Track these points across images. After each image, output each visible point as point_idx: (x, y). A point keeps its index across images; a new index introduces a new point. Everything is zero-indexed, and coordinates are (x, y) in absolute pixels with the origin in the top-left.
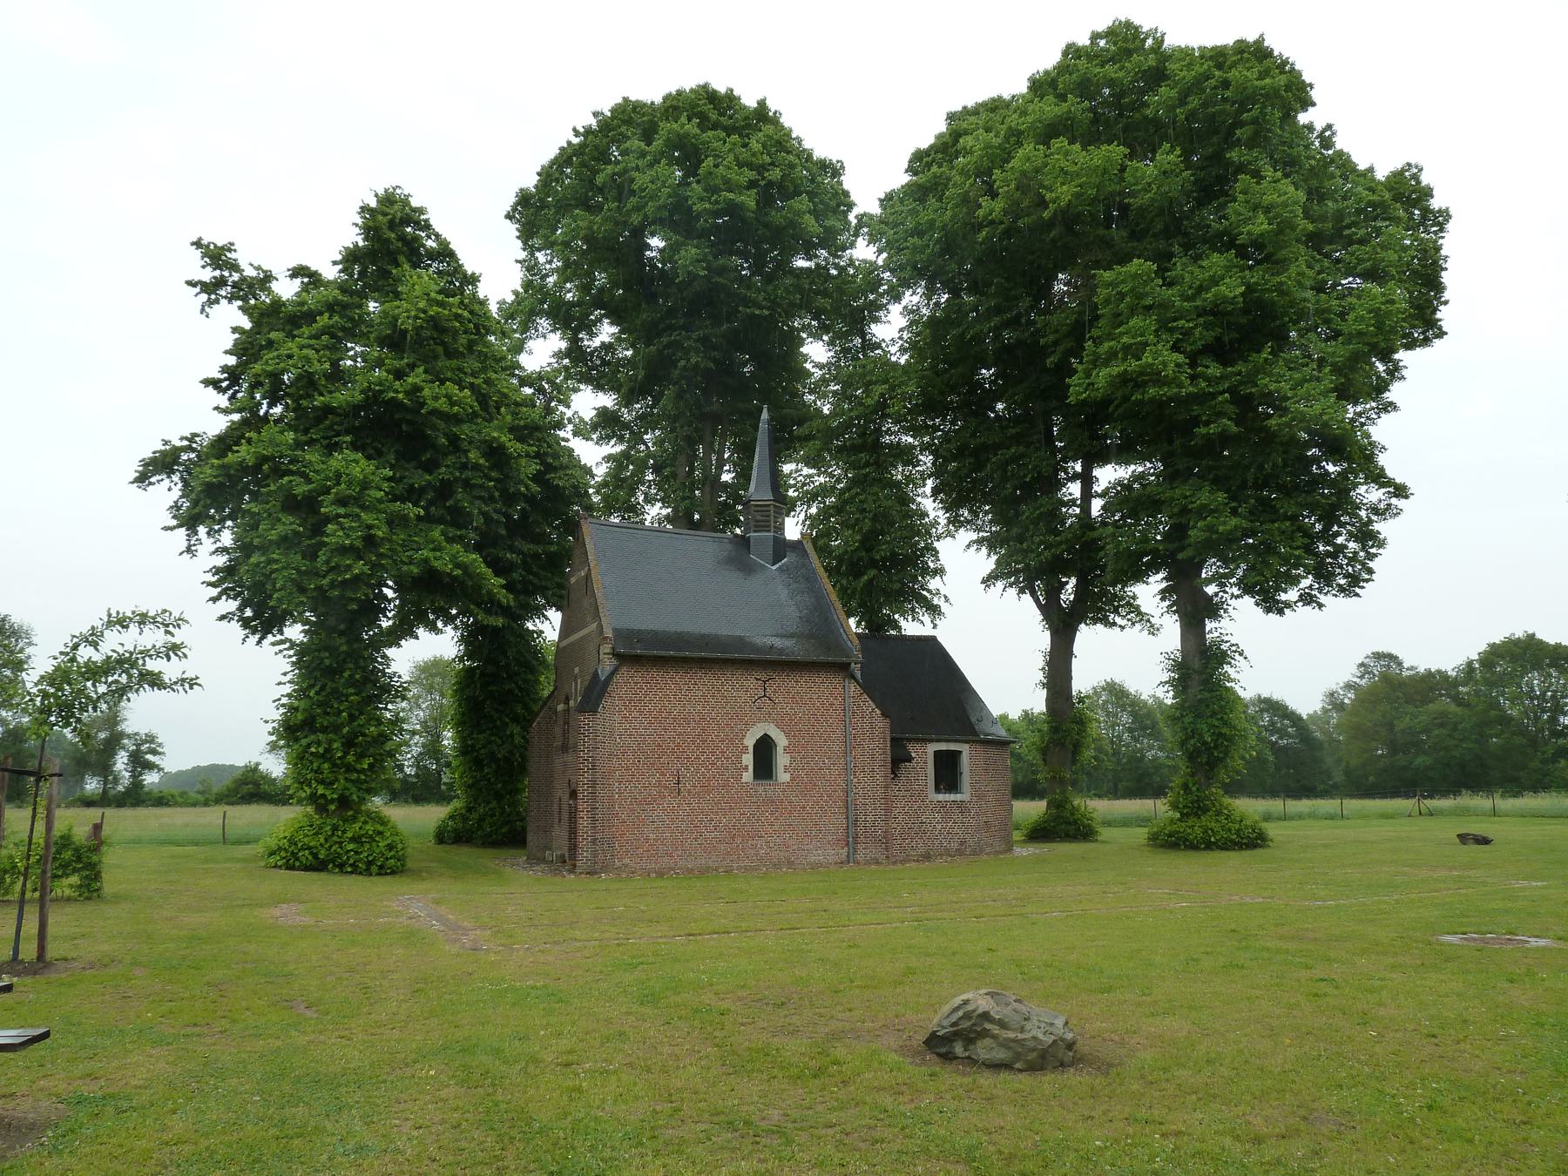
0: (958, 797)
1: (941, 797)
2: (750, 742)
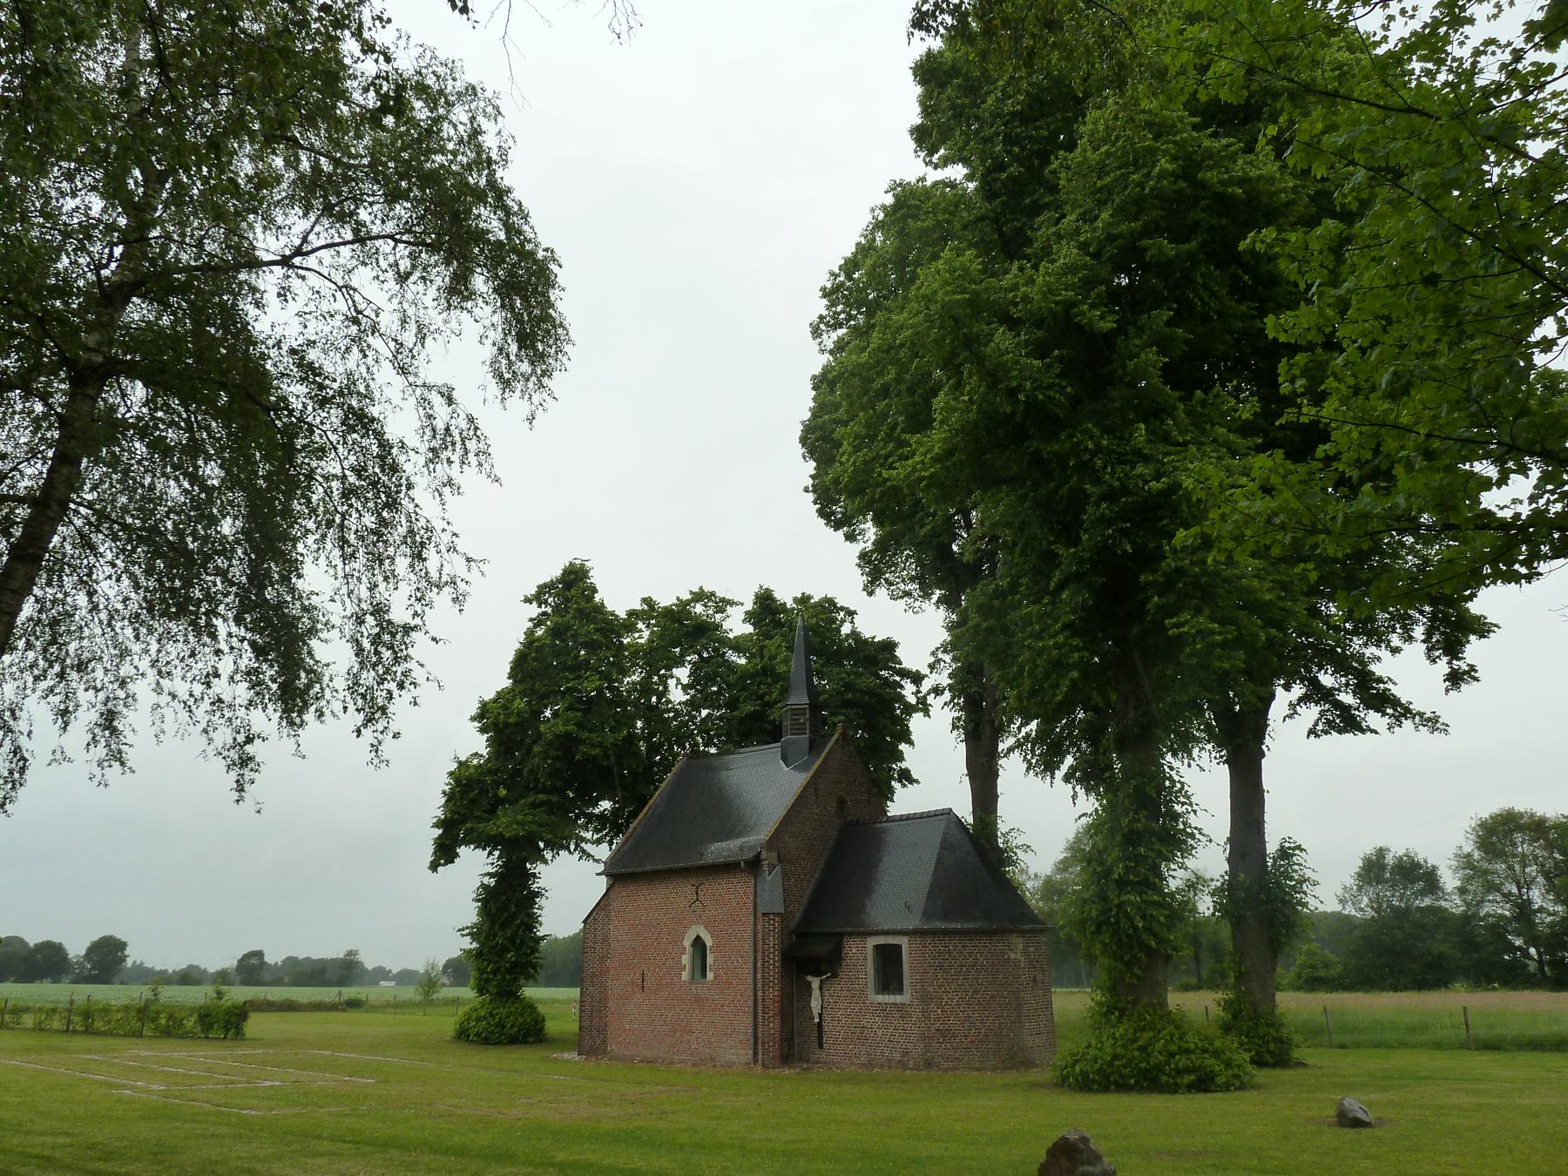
0: (898, 999)
1: (882, 998)
2: (687, 943)
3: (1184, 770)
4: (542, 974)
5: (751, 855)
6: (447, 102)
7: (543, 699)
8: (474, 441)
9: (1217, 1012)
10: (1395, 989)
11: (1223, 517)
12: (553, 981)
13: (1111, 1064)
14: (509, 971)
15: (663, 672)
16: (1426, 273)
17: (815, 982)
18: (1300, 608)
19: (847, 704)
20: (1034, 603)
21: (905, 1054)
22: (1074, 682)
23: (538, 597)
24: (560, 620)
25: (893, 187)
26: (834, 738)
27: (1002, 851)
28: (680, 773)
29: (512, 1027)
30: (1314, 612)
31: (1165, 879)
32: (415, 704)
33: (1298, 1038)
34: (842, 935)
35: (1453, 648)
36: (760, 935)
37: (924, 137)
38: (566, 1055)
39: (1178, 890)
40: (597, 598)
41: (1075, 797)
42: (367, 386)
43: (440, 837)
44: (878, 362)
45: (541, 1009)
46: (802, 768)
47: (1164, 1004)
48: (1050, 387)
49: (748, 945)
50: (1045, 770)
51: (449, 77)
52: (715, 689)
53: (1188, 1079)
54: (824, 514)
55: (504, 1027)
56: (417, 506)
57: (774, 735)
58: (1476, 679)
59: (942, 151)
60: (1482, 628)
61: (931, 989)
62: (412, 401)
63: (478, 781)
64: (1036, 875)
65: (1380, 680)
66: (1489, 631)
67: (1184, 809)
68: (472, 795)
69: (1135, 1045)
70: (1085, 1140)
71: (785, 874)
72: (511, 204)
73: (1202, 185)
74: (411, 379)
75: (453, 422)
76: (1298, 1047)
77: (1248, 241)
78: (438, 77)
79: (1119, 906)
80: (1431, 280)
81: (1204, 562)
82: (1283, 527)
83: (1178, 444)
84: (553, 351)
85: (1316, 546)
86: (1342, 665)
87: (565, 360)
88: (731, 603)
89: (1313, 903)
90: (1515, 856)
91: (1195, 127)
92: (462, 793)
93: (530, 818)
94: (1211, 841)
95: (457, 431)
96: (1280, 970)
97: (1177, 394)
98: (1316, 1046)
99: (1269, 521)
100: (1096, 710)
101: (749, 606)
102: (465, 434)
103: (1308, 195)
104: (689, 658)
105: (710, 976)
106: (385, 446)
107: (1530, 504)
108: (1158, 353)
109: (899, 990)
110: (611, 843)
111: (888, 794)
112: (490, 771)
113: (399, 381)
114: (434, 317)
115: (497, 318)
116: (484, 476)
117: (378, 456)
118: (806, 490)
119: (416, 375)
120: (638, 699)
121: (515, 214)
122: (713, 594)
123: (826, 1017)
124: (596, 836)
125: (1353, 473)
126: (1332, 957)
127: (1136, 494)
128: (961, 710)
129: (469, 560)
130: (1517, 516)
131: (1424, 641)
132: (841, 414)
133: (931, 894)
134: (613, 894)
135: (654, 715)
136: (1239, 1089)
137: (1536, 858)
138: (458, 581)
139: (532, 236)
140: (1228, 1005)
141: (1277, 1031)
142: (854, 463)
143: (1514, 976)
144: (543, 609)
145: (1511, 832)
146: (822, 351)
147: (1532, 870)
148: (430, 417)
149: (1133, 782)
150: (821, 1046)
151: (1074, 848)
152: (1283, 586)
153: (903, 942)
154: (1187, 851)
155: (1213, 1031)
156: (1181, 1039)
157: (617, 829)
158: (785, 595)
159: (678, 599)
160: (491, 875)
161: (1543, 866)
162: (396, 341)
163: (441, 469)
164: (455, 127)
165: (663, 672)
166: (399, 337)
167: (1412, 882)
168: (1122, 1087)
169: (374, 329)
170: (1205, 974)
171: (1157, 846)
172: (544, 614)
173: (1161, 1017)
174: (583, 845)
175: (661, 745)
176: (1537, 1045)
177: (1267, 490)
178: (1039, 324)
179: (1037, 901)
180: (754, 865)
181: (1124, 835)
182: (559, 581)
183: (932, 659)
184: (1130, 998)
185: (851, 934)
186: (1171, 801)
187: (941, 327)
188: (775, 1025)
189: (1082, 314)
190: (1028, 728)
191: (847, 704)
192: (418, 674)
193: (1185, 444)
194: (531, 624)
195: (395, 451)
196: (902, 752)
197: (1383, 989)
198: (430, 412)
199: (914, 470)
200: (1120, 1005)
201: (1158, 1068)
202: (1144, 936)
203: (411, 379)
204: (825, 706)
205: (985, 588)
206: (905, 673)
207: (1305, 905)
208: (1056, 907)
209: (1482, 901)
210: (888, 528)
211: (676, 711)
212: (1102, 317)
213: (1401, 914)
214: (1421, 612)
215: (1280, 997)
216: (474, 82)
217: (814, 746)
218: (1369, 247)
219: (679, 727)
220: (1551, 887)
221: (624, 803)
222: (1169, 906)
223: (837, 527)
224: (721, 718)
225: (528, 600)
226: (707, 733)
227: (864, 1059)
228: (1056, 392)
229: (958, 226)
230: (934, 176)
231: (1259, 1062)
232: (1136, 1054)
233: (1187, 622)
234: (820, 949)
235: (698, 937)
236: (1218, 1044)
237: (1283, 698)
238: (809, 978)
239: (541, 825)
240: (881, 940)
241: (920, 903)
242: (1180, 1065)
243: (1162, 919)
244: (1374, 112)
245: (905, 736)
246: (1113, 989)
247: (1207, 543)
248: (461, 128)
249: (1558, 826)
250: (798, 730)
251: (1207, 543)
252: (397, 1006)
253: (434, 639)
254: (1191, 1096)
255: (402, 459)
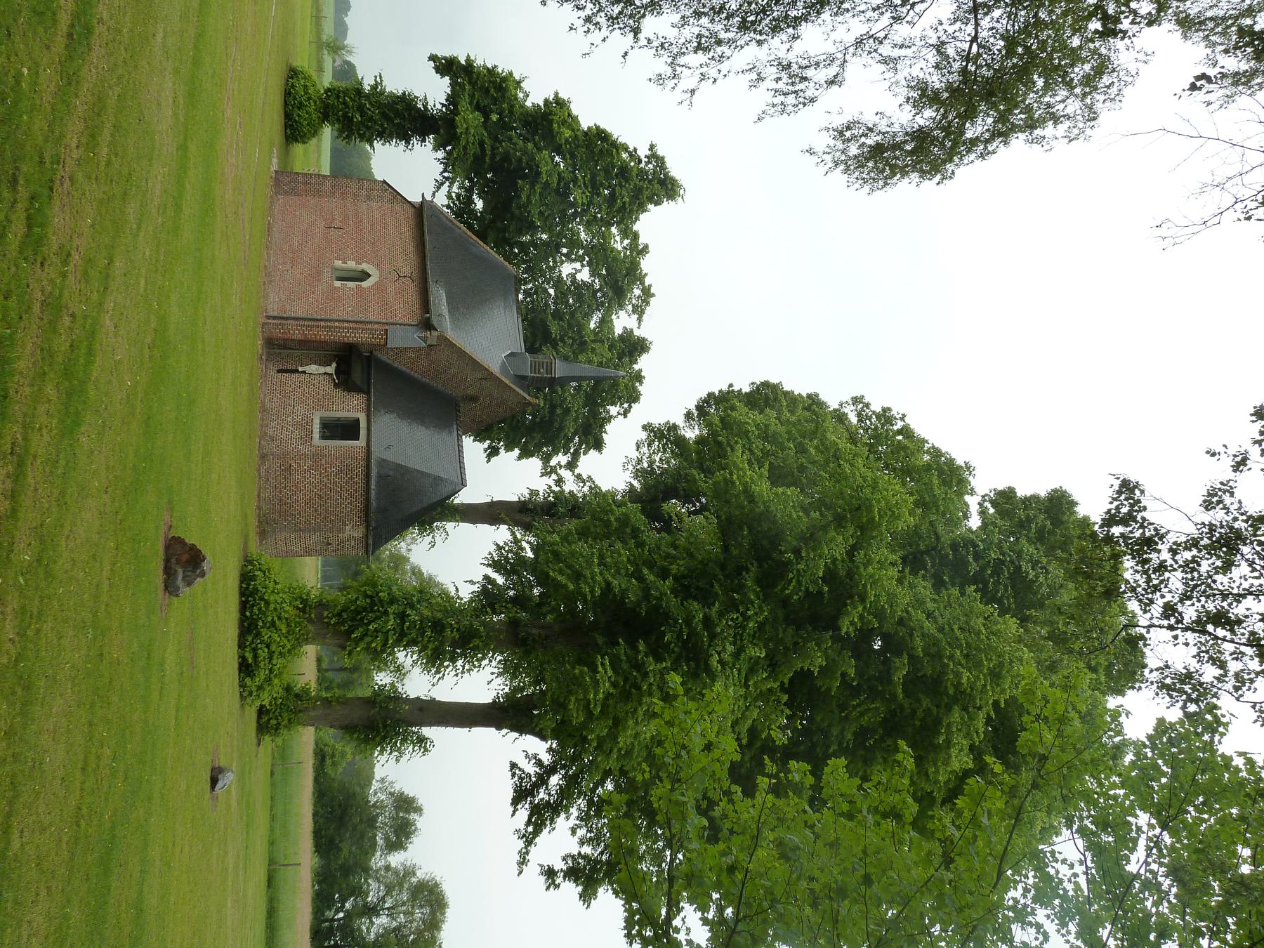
0: (316, 435)
1: (317, 422)
2: (365, 267)
3: (489, 669)
4: (341, 143)
5: (435, 322)
6: (1085, 95)
7: (571, 156)
8: (794, 101)
9: (300, 683)
10: (315, 815)
11: (687, 713)
12: (336, 154)
13: (262, 599)
14: (345, 115)
15: (587, 259)
16: (873, 877)
17: (331, 369)
18: (612, 764)
19: (553, 407)
20: (629, 560)
21: (272, 439)
22: (565, 586)
23: (654, 156)
24: (634, 174)
25: (968, 467)
26: (528, 397)
27: (431, 524)
28: (504, 268)
29: (299, 116)
30: (606, 774)
31: (405, 649)
32: (571, 29)
33: (279, 741)
34: (368, 393)
35: (573, 873)
36: (369, 326)
37: (1005, 499)
38: (275, 160)
39: (395, 660)
40: (650, 206)
41: (472, 582)
42: (848, 10)
43: (459, 62)
44: (826, 448)
45: (314, 141)
46: (504, 368)
47: (307, 641)
48: (799, 583)
49: (361, 316)
50: (494, 561)
51: (1107, 97)
52: (571, 301)
53: (249, 656)
54: (711, 398)
55: (299, 108)
56: (742, 47)
57: (531, 348)
58: (548, 888)
59: (992, 511)
60: (587, 896)
61: (323, 461)
62: (832, 49)
63: (503, 97)
64: (410, 550)
65: (552, 821)
66: (584, 901)
67: (459, 667)
68: (492, 91)
69: (276, 618)
70: (203, 574)
71: (419, 349)
72: (995, 144)
73: (949, 708)
74: (851, 50)
75: (812, 84)
76: (273, 741)
77: (905, 747)
78: (1108, 87)
79: (386, 613)
80: (867, 880)
81: (650, 695)
82: (678, 756)
83: (747, 680)
84: (865, 176)
85: (661, 780)
86: (566, 794)
87: (857, 186)
88: (640, 320)
89: (383, 759)
90: (413, 907)
91: (996, 703)
92: (494, 83)
93: (471, 140)
94: (433, 685)
95: (804, 88)
96: (332, 731)
97: (786, 681)
98: (273, 754)
99: (684, 747)
100: (540, 605)
101: (637, 333)
102: (801, 94)
103: (932, 792)
104: (597, 281)
105: (338, 284)
106: (797, 22)
107: (686, 940)
108: (820, 667)
109: (323, 437)
110: (448, 207)
111: (479, 437)
112: (512, 106)
113: (850, 39)
114: (904, 72)
115: (896, 128)
116: (764, 108)
117: (787, 16)
118: (731, 385)
119: (854, 54)
120: (565, 237)
121: (986, 148)
122: (648, 304)
123: (302, 377)
124: (454, 195)
125: (717, 812)
126: (340, 770)
127: (710, 645)
128: (545, 498)
129: (693, 92)
130: (677, 930)
131: (579, 853)
132: (786, 414)
133: (399, 467)
134: (406, 206)
135: (552, 248)
136: (241, 695)
137: (411, 922)
138: (676, 81)
139: (966, 162)
140: (306, 691)
141: (286, 726)
142: (748, 423)
143: (322, 901)
144: (644, 160)
145: (431, 906)
146: (841, 405)
147: (402, 918)
148: (817, 64)
149: (482, 629)
150: (279, 371)
151: (431, 580)
152: (629, 753)
153: (361, 442)
154: (426, 669)
155: (286, 678)
156: (281, 653)
157: (459, 214)
158: (644, 363)
159: (646, 274)
160: (425, 106)
161: (405, 927)
162: (885, 38)
163: (772, 72)
164: (1063, 101)
165: (587, 259)
166: (887, 41)
167: (395, 832)
168: (244, 606)
169: (897, 19)
170: (330, 675)
171: (431, 646)
172: (640, 161)
173: (297, 639)
174: (447, 184)
175: (527, 254)
176: (271, 912)
177: (708, 747)
178: (850, 575)
179: (390, 550)
180: (427, 325)
181: (440, 620)
182: (666, 175)
183: (585, 477)
184: (313, 615)
185: (369, 400)
186: (466, 657)
187: (852, 497)
188: (297, 335)
189: (856, 608)
190: (528, 550)
191: (553, 407)
192: (596, 36)
193: (746, 686)
194: (631, 149)
195: (791, 31)
196: (512, 450)
197: (315, 805)
198: (821, 65)
199: (739, 469)
200: (308, 609)
201: (258, 635)
202: (361, 629)
203: (851, 50)
204: (552, 391)
205: (639, 519)
206: (576, 456)
207: (381, 753)
208: (384, 565)
209: (379, 882)
210: (694, 447)
211: (554, 268)
212: (852, 623)
213: (371, 822)
214: (602, 853)
215: (312, 729)
216: (1100, 120)
217: (521, 379)
218: (893, 836)
219: (541, 270)
220: (388, 931)
221: (480, 219)
222: (383, 651)
223: (699, 408)
224: (546, 304)
225: (652, 147)
226: (536, 292)
227: (268, 405)
228: (794, 587)
229: (933, 518)
230: (973, 502)
231: (261, 711)
232: (269, 619)
233: (606, 672)
234: (357, 375)
235: (369, 276)
236: (276, 681)
237: (540, 748)
238: (334, 365)
239: (465, 148)
240: (363, 424)
241: (390, 456)
242: (260, 651)
243: (374, 645)
244: (1000, 848)
245: (525, 454)
246: (321, 605)
247: (667, 698)
248: (1061, 106)
249: (434, 940)
250: (534, 367)
251: (667, 698)
252: (318, 19)
253: (626, 54)
254: (236, 657)
255: (784, 37)
